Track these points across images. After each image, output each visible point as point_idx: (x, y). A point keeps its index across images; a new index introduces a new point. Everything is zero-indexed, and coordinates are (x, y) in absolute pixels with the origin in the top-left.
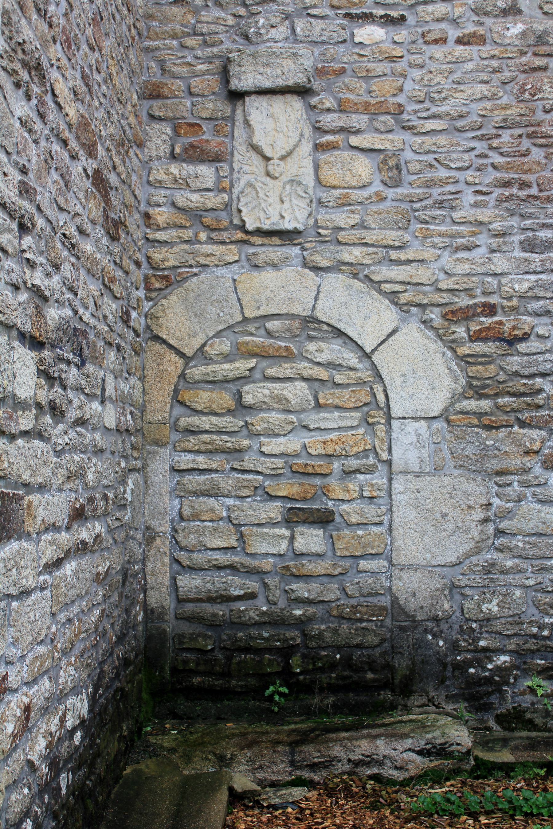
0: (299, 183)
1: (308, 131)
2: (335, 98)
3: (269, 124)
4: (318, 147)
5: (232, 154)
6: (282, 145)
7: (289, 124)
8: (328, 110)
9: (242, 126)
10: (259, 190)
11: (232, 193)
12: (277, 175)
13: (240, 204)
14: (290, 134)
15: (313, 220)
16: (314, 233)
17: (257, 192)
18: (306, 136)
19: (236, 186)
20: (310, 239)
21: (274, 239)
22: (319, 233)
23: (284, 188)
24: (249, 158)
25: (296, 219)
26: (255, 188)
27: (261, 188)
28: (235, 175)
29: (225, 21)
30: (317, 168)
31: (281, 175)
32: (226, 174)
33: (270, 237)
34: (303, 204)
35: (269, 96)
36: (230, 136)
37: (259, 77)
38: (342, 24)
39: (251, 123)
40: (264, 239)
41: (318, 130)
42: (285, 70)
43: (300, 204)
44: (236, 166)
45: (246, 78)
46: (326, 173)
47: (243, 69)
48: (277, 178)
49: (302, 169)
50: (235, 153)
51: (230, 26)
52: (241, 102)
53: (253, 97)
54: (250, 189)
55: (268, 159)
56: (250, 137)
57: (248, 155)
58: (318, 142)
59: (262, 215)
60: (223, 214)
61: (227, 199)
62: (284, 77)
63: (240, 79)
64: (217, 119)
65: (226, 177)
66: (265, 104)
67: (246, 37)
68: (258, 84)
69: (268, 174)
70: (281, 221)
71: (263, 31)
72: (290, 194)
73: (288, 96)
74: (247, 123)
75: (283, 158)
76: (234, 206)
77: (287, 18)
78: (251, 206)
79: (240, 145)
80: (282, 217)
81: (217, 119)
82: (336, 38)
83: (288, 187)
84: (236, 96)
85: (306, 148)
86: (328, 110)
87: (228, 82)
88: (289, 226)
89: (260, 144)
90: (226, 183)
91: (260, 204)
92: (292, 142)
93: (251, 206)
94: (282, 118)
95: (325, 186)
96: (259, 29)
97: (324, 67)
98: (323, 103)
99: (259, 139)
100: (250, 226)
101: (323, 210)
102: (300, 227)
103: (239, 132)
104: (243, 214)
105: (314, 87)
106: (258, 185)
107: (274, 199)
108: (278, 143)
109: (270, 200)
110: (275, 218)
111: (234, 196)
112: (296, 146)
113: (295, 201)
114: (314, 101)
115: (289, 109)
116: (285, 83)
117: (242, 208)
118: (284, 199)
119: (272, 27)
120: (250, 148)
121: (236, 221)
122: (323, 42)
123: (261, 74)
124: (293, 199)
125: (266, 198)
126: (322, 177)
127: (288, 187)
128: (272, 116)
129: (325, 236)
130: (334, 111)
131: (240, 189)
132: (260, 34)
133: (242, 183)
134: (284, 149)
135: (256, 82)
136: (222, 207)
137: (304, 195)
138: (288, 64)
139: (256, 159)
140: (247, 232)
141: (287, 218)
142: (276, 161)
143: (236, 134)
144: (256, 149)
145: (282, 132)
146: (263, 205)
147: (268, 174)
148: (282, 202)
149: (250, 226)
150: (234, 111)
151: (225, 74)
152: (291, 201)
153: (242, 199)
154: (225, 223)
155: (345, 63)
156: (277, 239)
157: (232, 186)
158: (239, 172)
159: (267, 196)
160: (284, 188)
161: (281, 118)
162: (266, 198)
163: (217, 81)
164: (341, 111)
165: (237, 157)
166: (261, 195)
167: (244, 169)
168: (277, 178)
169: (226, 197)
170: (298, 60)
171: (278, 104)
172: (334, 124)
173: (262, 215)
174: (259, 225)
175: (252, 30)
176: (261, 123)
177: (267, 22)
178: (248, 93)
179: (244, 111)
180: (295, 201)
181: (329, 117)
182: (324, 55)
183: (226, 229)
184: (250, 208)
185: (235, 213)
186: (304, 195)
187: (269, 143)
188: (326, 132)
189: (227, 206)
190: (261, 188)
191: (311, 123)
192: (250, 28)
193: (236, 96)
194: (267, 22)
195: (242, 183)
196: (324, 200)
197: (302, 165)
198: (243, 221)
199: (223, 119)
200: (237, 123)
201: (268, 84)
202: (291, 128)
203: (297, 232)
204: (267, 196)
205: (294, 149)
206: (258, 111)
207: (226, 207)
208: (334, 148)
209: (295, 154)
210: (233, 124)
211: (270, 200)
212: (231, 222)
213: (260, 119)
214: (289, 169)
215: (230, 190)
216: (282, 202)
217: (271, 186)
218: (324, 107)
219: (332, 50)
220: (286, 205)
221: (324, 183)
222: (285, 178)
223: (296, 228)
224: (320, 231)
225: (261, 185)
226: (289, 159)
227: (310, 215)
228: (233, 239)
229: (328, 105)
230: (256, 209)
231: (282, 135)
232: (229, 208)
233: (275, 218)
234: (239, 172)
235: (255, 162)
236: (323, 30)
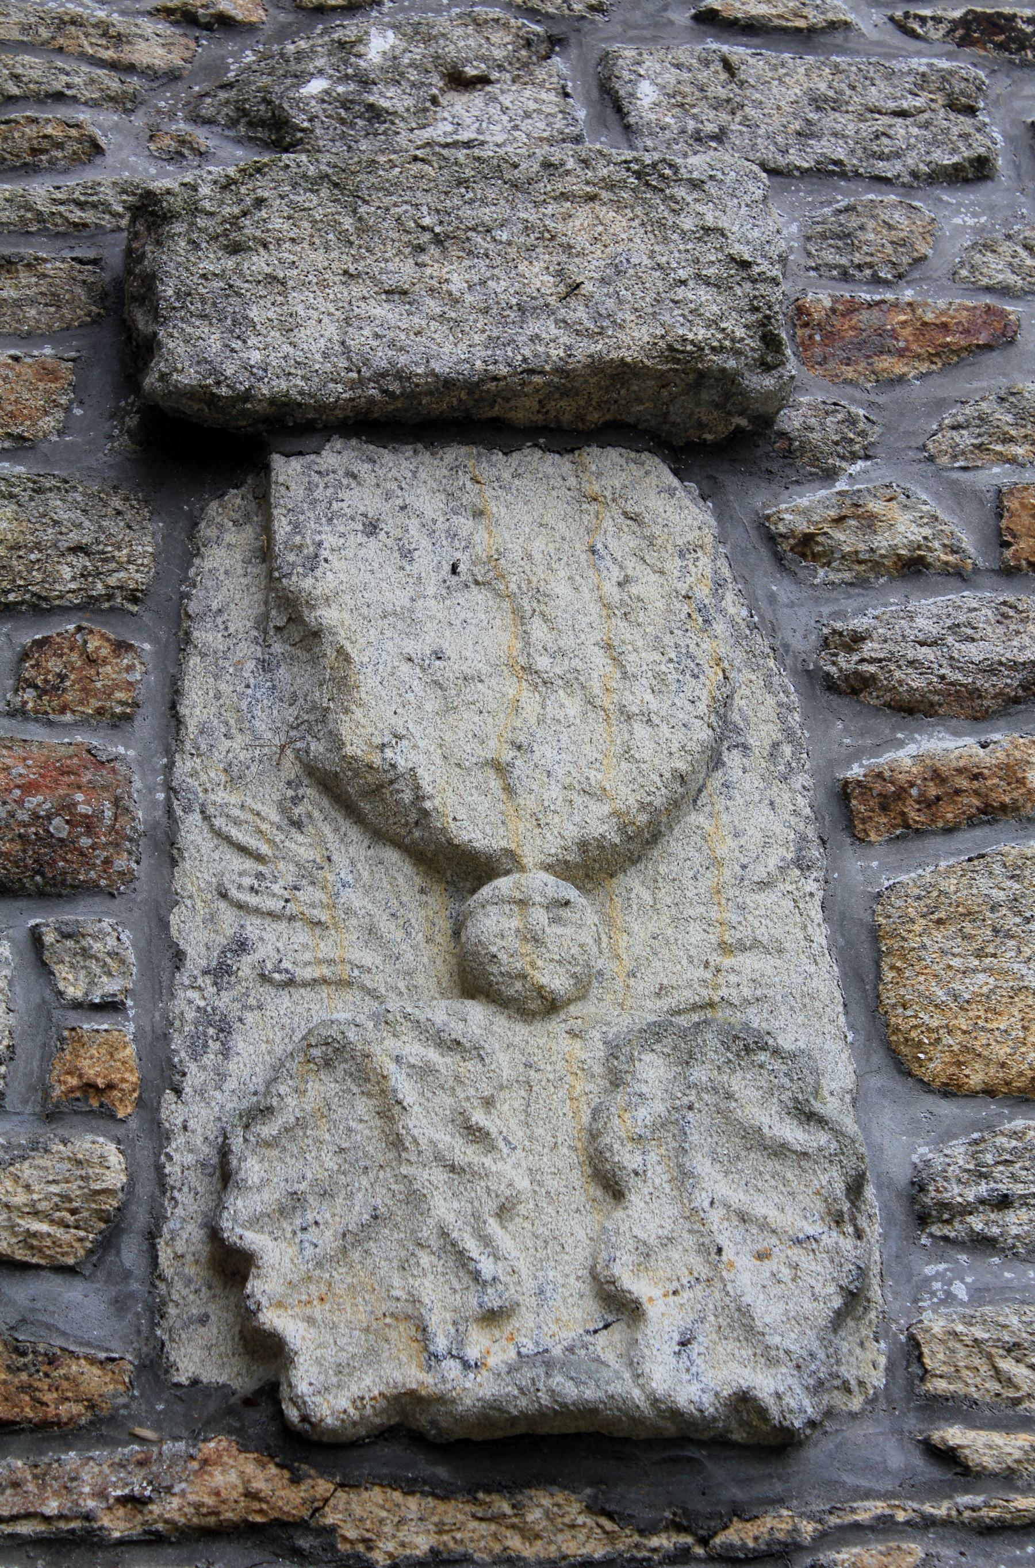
0: (749, 1046)
1: (766, 707)
2: (959, 496)
3: (475, 634)
4: (852, 811)
5: (168, 850)
6: (579, 774)
7: (623, 630)
8: (912, 567)
9: (247, 650)
10: (406, 1088)
11: (160, 1135)
12: (555, 981)
13: (241, 1206)
14: (640, 696)
15: (879, 1353)
16: (899, 1457)
17: (389, 1109)
18: (762, 733)
19: (195, 1077)
20: (868, 1510)
21: (540, 1506)
22: (947, 1457)
23: (616, 1081)
24: (308, 873)
25: (743, 1323)
26: (366, 1076)
27: (424, 1072)
28: (189, 1001)
29: (119, 40)
30: (867, 957)
31: (582, 990)
32: (111, 986)
33: (512, 1487)
34: (792, 1206)
35: (453, 454)
36: (147, 725)
37: (381, 310)
38: (946, 76)
39: (329, 616)
40: (453, 1511)
41: (845, 686)
42: (588, 270)
43: (762, 1208)
44: (196, 935)
45: (289, 314)
46: (940, 982)
47: (259, 263)
48: (550, 1005)
49: (750, 962)
50: (193, 832)
51: (150, 73)
52: (235, 498)
53: (335, 456)
54: (322, 1087)
55: (459, 870)
56: (318, 720)
57: (302, 847)
58: (856, 771)
59: (438, 1295)
60: (81, 1309)
61: (115, 1178)
62: (579, 313)
63: (239, 327)
64: (41, 608)
65: (110, 1006)
66: (429, 503)
67: (274, 130)
68: (381, 358)
69: (473, 979)
70: (607, 1346)
71: (387, 97)
72: (673, 1125)
73: (611, 468)
74: (290, 624)
75: (594, 867)
76: (183, 1236)
77: (555, 42)
78: (331, 1220)
79: (234, 778)
80: (620, 1307)
81: (41, 608)
82: (913, 147)
83: (653, 1071)
84: (206, 449)
85: (762, 814)
86: (912, 567)
87: (139, 351)
88: (680, 1372)
89: (402, 758)
90: (111, 1054)
91: (415, 1199)
92: (668, 743)
93: (331, 1220)
94: (573, 596)
95: (951, 1090)
96: (365, 82)
97: (853, 308)
98: (870, 522)
99: (387, 719)
100: (333, 1380)
101: (957, 1277)
102: (781, 1391)
103: (227, 693)
104: (262, 1287)
105: (791, 421)
106: (397, 1053)
107: (533, 1160)
108: (545, 753)
109: (509, 1171)
110: (558, 1318)
111: (184, 1157)
112: (686, 793)
113: (714, 1182)
114: (801, 507)
115: (620, 543)
116: (585, 349)
117: (253, 1239)
118: (629, 1158)
119: (460, 81)
120: (312, 803)
121: (198, 1357)
122: (827, 172)
123: (396, 293)
124: (702, 1165)
125: (466, 1153)
126: (913, 1020)
127: (653, 1071)
128: (489, 578)
129: (1008, 1478)
130: (959, 575)
131: (227, 1101)
132: (375, 113)
133: (250, 1056)
134: (596, 793)
135: (360, 339)
136: (72, 1242)
137: (793, 1134)
138: (608, 235)
139: (370, 889)
140: (299, 1445)
141: (664, 1317)
142: (541, 883)
143: (196, 708)
144: (364, 799)
145: (573, 682)
146: (444, 1208)
147: (473, 979)
148: (611, 1185)
149: (333, 1380)
150: (183, 552)
151: (122, 317)
152: (683, 1177)
153: (251, 1168)
154: (94, 1380)
155: (1004, 291)
156: (574, 1510)
157: (164, 1076)
158: (221, 973)
159: (475, 1134)
160: (616, 1081)
161: (560, 588)
162: (466, 1153)
163: (48, 373)
164: (1008, 572)
165: (203, 862)
166: (425, 1124)
167: (264, 952)
168: (550, 1005)
169: (108, 1160)
170: (678, 208)
171: (529, 511)
172: (974, 652)
173: (438, 1295)
174: (412, 1375)
175: (316, 86)
176: (408, 620)
177: (418, 51)
178: (297, 424)
179: (265, 553)
180: (714, 1182)
181: (928, 610)
182: (846, 238)
183: (100, 1427)
184: (327, 1239)
185: (187, 1290)
186: (793, 1134)
187: (472, 752)
188: (913, 710)
189: (114, 1234)
190: (424, 1072)
191: (780, 651)
192: (301, 78)
193: (206, 449)
194: (418, 51)
195: (250, 1056)
196: (955, 1193)
197: (747, 914)
198: (266, 1350)
199: (90, 605)
200: (205, 636)
201: (448, 350)
202: (641, 658)
203: (753, 1442)
204: (475, 1134)
205: (675, 807)
206: (375, 549)
207: (108, 1242)
208: (991, 813)
209: (680, 852)
210: (180, 643)
211: (509, 1171)
212: (154, 1366)
213: (401, 598)
214: (649, 948)
215: (148, 1107)
216: (611, 1185)
217: (505, 1064)
218: (882, 542)
219: (888, 220)
220: (647, 1214)
221: (937, 1066)
222: (610, 1014)
223: (743, 1401)
224: (954, 1435)
225: (416, 1050)
226: (633, 884)
227: (854, 1299)
228: (170, 1509)
229: (903, 530)
230: (386, 1246)
231: (573, 707)
232: (130, 1253)
233: (558, 1318)
234: (221, 973)
235: (355, 898)
236: (818, 102)
